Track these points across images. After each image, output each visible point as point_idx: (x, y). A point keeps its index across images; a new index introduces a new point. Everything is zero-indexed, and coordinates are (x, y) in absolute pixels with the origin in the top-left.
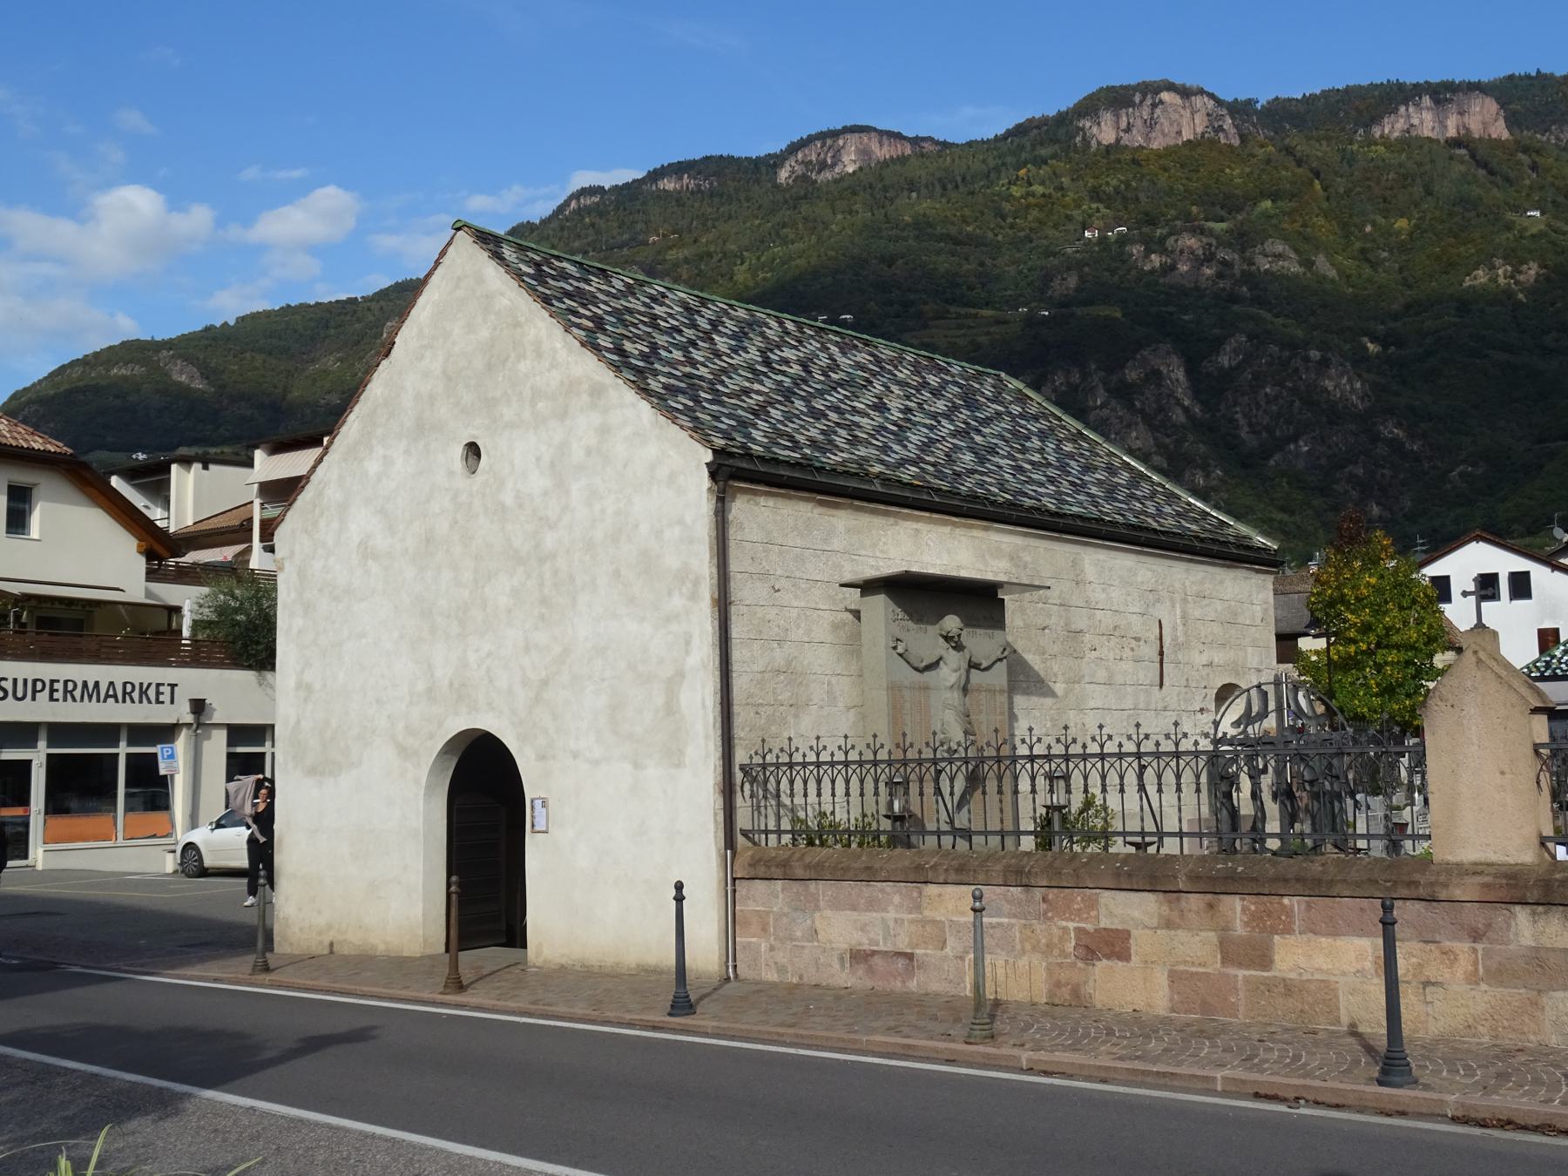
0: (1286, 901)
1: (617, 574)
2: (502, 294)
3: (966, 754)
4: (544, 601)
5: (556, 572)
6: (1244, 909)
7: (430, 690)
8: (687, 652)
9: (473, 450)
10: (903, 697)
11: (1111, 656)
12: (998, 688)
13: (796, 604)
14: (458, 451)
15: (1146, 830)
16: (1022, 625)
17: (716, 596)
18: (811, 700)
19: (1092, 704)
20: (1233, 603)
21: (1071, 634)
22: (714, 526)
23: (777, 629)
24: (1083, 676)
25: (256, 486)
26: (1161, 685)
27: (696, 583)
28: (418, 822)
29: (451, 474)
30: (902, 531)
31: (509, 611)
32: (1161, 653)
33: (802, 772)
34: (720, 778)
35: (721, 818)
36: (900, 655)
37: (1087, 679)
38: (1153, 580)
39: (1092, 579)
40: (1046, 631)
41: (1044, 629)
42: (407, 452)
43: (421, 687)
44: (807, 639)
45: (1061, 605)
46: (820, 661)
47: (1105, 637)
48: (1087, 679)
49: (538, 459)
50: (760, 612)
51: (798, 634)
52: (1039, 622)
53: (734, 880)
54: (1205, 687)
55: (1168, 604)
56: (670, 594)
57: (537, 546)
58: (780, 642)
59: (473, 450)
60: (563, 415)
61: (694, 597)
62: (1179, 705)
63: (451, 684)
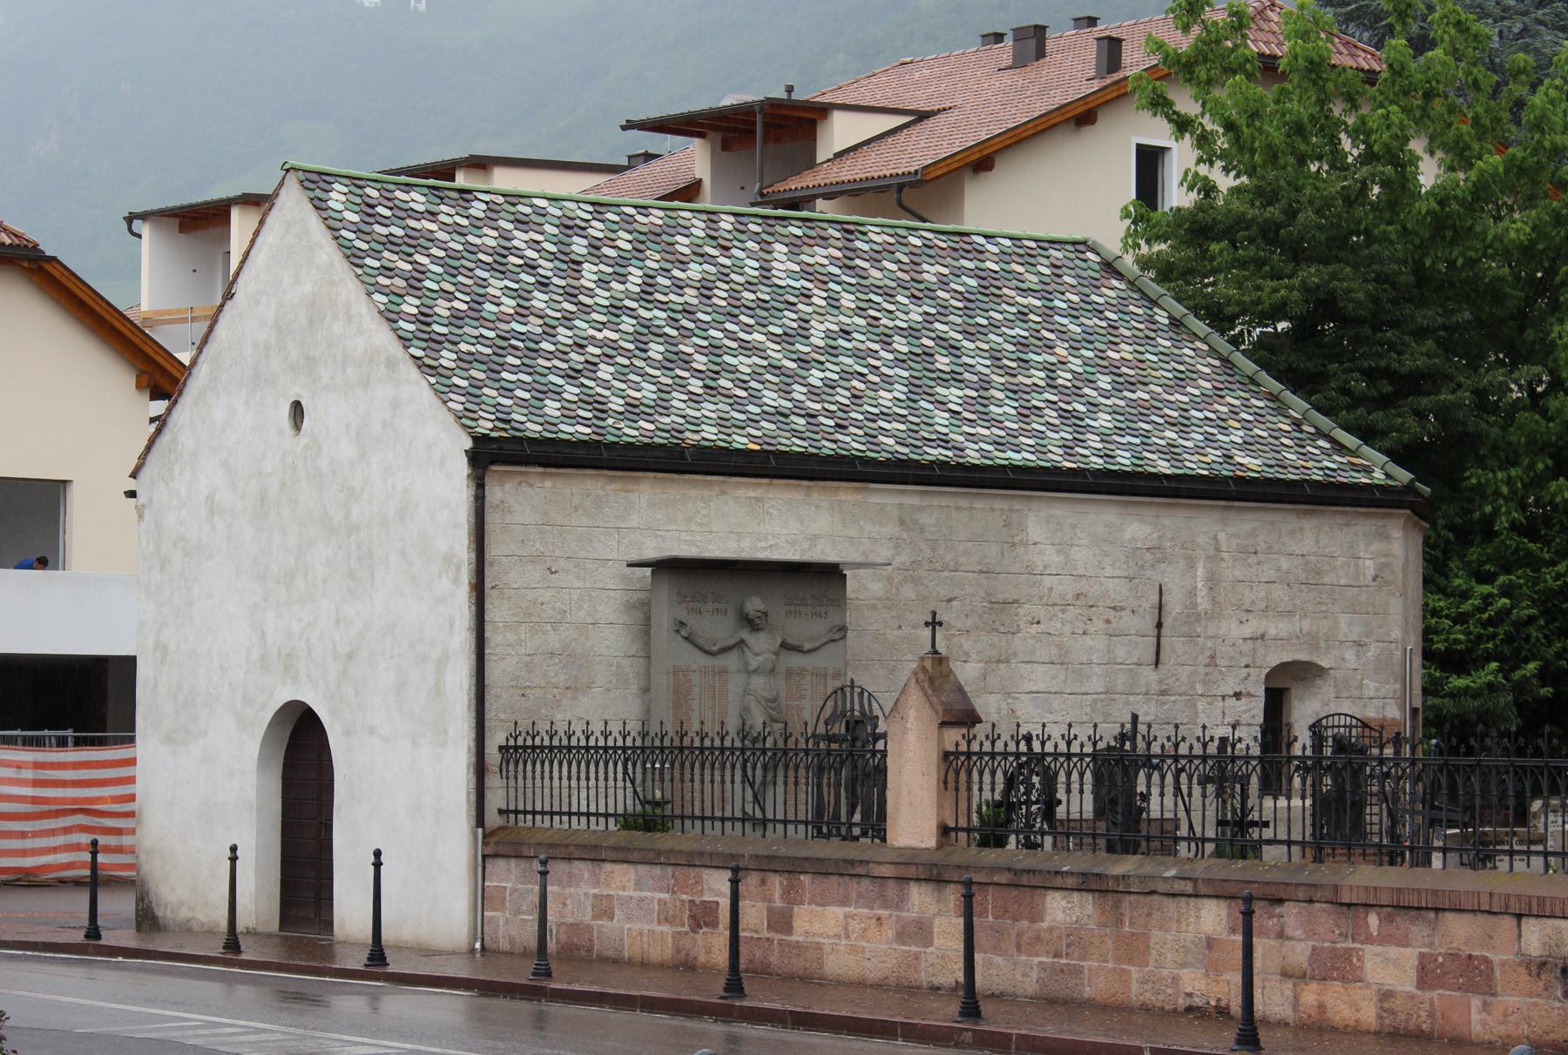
0: (802, 877)
1: (403, 553)
2: (322, 248)
3: (681, 742)
4: (351, 574)
5: (359, 546)
6: (781, 884)
7: (263, 658)
8: (451, 634)
9: (297, 410)
10: (689, 681)
11: (1067, 629)
12: (830, 672)
13: (578, 585)
14: (286, 410)
15: (1285, 848)
16: (913, 596)
17: (474, 581)
18: (594, 683)
19: (1028, 687)
20: (1313, 559)
21: (996, 606)
22: (473, 511)
23: (551, 612)
24: (1015, 654)
25: (185, 358)
26: (1157, 663)
27: (458, 568)
28: (251, 794)
29: (281, 432)
30: (731, 503)
31: (325, 581)
32: (1159, 625)
33: (1065, 765)
34: (473, 759)
35: (473, 797)
36: (685, 638)
37: (1021, 657)
38: (1155, 536)
39: (1037, 540)
40: (954, 603)
41: (950, 600)
42: (247, 403)
43: (255, 655)
44: (590, 621)
45: (981, 572)
46: (607, 643)
47: (1059, 608)
48: (1021, 657)
49: (348, 427)
50: (530, 595)
51: (581, 615)
52: (943, 593)
53: (484, 857)
54: (1247, 666)
55: (1182, 564)
56: (440, 576)
57: (347, 516)
58: (555, 625)
59: (297, 410)
60: (366, 384)
61: (456, 581)
62: (1193, 688)
63: (279, 654)
